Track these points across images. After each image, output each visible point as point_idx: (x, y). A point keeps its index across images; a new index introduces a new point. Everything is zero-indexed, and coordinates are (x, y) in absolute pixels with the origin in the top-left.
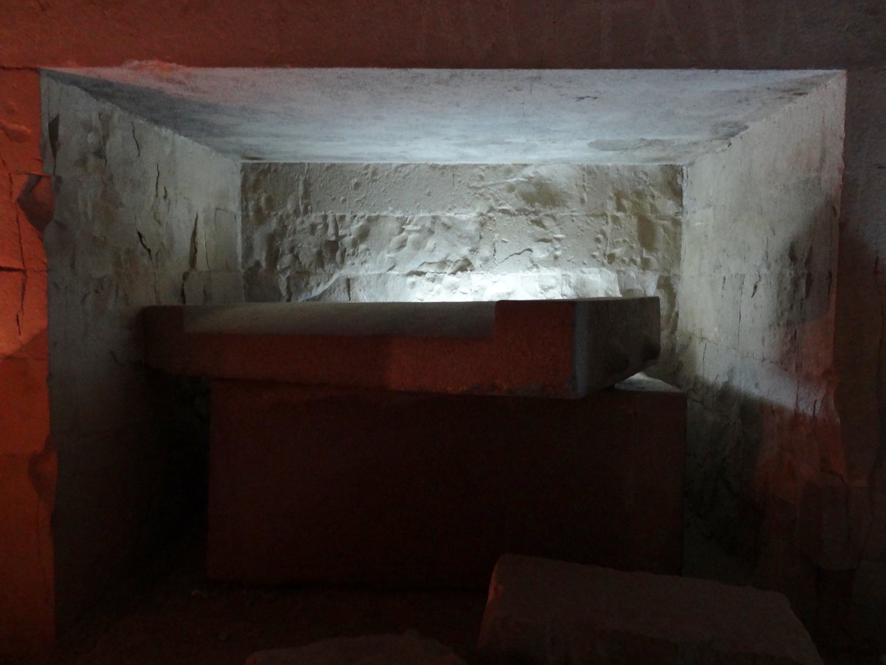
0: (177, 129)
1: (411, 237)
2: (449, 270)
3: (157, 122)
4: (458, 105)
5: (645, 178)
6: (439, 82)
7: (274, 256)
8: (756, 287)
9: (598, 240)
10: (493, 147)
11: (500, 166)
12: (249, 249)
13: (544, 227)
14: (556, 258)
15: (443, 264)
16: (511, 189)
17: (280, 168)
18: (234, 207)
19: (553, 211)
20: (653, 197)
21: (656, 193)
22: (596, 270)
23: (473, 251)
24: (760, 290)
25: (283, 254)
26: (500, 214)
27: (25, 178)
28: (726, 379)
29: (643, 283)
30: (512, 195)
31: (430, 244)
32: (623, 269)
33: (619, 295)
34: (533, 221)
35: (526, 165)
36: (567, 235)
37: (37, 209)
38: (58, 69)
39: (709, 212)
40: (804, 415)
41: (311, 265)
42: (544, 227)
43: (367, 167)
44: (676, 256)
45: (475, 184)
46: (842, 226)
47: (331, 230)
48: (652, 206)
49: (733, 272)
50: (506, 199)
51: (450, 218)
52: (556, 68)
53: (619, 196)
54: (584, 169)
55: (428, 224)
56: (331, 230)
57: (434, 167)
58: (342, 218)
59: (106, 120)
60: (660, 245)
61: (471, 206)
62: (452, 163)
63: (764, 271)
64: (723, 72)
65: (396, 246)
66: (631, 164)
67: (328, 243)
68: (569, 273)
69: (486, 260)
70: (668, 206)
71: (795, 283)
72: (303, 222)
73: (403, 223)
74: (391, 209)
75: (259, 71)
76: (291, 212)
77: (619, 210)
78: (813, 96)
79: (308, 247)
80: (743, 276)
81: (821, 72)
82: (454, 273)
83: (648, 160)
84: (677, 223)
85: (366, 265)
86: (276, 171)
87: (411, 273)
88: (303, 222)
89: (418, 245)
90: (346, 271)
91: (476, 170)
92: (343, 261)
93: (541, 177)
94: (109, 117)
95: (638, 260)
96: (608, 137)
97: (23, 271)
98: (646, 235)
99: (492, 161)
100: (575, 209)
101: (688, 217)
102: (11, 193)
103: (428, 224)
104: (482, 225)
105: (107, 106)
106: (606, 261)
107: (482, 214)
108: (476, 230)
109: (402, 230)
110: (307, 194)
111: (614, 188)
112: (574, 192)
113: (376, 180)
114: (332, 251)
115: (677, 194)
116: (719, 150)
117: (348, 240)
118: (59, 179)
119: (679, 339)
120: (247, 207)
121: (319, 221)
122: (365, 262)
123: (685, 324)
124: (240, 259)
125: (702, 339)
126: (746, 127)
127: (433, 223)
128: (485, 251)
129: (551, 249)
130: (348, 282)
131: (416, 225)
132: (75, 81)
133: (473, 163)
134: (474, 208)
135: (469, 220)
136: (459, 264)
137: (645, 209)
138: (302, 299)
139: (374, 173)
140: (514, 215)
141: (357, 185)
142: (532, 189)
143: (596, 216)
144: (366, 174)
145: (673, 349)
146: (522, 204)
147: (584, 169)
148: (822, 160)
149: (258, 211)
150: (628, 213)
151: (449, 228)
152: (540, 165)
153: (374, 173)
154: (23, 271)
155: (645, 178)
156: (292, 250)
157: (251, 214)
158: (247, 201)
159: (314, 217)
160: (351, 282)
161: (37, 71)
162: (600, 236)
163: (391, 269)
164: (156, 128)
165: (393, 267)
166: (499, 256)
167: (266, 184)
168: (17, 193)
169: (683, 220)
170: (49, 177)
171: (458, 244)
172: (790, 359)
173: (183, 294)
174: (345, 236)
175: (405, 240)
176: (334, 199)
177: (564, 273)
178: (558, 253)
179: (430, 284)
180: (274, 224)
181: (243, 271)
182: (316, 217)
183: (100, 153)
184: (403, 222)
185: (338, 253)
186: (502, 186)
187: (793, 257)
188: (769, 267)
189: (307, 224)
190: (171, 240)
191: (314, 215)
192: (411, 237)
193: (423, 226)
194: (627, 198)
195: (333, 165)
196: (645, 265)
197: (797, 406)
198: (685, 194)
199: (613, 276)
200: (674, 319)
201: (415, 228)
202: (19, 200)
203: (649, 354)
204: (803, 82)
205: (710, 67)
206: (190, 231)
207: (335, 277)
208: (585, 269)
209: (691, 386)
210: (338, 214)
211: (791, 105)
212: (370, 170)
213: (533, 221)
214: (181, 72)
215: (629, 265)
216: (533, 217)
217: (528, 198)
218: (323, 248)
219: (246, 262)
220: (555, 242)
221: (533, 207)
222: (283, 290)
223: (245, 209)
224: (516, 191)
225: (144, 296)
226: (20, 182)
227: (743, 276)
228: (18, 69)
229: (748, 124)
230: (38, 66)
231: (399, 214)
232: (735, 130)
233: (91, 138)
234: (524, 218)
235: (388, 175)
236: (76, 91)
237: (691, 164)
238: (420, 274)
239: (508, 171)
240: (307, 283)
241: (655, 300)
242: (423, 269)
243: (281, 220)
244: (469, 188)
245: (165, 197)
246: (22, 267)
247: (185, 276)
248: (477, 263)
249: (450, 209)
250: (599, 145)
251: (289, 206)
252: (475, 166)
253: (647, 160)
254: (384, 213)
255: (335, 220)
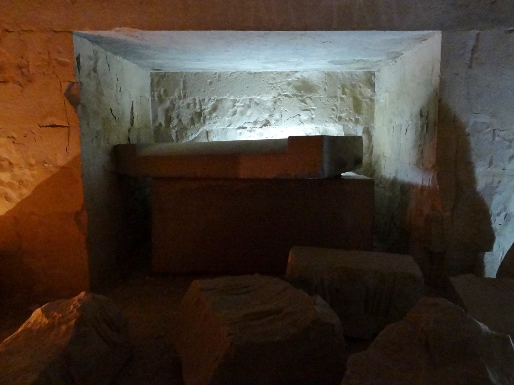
0: (124, 57)
1: (239, 109)
2: (259, 126)
3: (116, 54)
4: (266, 45)
5: (356, 77)
6: (259, 36)
7: (169, 120)
8: (407, 130)
9: (333, 110)
10: (281, 63)
11: (284, 72)
12: (155, 117)
13: (306, 103)
14: (312, 119)
15: (256, 123)
16: (289, 84)
17: (170, 74)
18: (148, 95)
19: (311, 95)
20: (360, 87)
21: (362, 85)
22: (332, 124)
23: (271, 116)
24: (408, 131)
25: (173, 119)
26: (284, 97)
27: (67, 84)
28: (394, 175)
29: (356, 131)
30: (290, 87)
31: (249, 112)
32: (346, 124)
33: (343, 134)
34: (300, 100)
35: (296, 72)
36: (317, 107)
37: (73, 98)
38: (80, 32)
39: (387, 94)
40: (425, 186)
41: (188, 124)
42: (306, 103)
43: (216, 73)
44: (372, 118)
45: (271, 82)
46: (440, 101)
47: (198, 106)
48: (360, 92)
49: (397, 124)
50: (287, 89)
51: (258, 99)
52: (313, 30)
53: (343, 87)
54: (326, 74)
55: (248, 103)
56: (198, 106)
57: (250, 73)
58: (204, 100)
59: (96, 53)
60: (364, 111)
61: (264, 93)
62: (259, 71)
63: (410, 122)
64: (388, 32)
65: (232, 114)
66: (349, 70)
67: (196, 113)
68: (319, 126)
69: (277, 120)
70: (368, 92)
71: (422, 127)
72: (183, 103)
73: (235, 102)
74: (228, 95)
75: (175, 32)
76: (177, 97)
77: (343, 94)
78: (429, 41)
79: (186, 116)
80: (401, 125)
81: (430, 31)
82: (261, 127)
83: (358, 69)
84: (372, 100)
85: (216, 124)
86: (168, 76)
87: (240, 128)
88: (183, 103)
89: (243, 114)
90: (206, 128)
91: (271, 75)
92: (204, 122)
93: (305, 78)
94: (97, 52)
95: (353, 119)
96: (337, 58)
97: (69, 127)
98: (357, 107)
99: (279, 70)
100: (321, 94)
101: (378, 97)
102: (61, 91)
103: (248, 103)
104: (275, 102)
105: (96, 47)
106: (337, 120)
107: (275, 97)
108: (272, 105)
109: (234, 106)
110: (185, 88)
111: (341, 83)
112: (322, 86)
113: (220, 80)
114: (199, 117)
115: (372, 85)
116: (391, 64)
117: (207, 111)
118: (81, 83)
119: (374, 158)
120: (154, 94)
121: (192, 102)
122: (216, 122)
123: (376, 151)
124: (151, 122)
125: (384, 157)
126: (402, 54)
127: (250, 102)
128: (277, 116)
129: (310, 114)
130: (207, 133)
131: (241, 103)
132: (86, 37)
133: (269, 71)
134: (271, 94)
135: (268, 100)
136: (264, 122)
137: (356, 93)
138: (184, 141)
139: (219, 76)
140: (291, 97)
141: (211, 83)
142: (300, 84)
143: (332, 97)
144: (215, 77)
145: (371, 164)
146: (295, 92)
147: (326, 74)
148: (433, 71)
149: (160, 96)
150: (348, 95)
151: (258, 104)
152: (304, 72)
153: (219, 76)
154: (69, 127)
155: (356, 77)
156: (178, 117)
157: (156, 98)
158: (154, 91)
159: (189, 100)
160: (209, 133)
161: (71, 33)
162: (334, 107)
163: (229, 126)
164: (115, 57)
165: (230, 125)
166: (284, 118)
167: (162, 82)
168: (64, 91)
169: (375, 99)
170: (77, 83)
171: (263, 112)
172: (420, 163)
173: (129, 139)
174: (205, 109)
175: (236, 111)
176: (199, 90)
177: (317, 126)
178: (313, 116)
179: (249, 133)
180: (168, 104)
181: (153, 128)
182: (190, 100)
183: (95, 70)
184: (235, 101)
185: (202, 118)
186: (284, 83)
187: (421, 116)
188: (412, 121)
189: (185, 104)
190: (123, 112)
191: (189, 99)
192: (239, 109)
193: (245, 104)
194: (348, 89)
195: (198, 73)
196: (357, 121)
197: (423, 183)
198: (376, 86)
199: (341, 127)
200: (371, 148)
201: (241, 105)
202: (65, 94)
203: (356, 163)
204: (424, 35)
205: (382, 30)
206: (131, 107)
207: (200, 130)
208: (327, 124)
209: (379, 181)
210: (201, 98)
211: (421, 44)
212: (217, 75)
213: (300, 100)
214: (138, 32)
215: (349, 122)
216: (301, 98)
217: (298, 89)
218: (194, 116)
219: (154, 124)
220: (312, 110)
221: (301, 93)
222: (174, 137)
223: (153, 96)
224: (292, 85)
225: (118, 138)
226: (65, 86)
227: (401, 125)
228: (63, 32)
229: (403, 52)
230: (72, 30)
231: (232, 98)
232: (398, 55)
233: (92, 63)
234: (296, 98)
235: (226, 78)
236: (85, 40)
237: (379, 71)
238: (244, 128)
239: (288, 75)
240: (186, 134)
241: (360, 138)
242: (245, 126)
243: (172, 102)
244: (268, 84)
245: (120, 91)
246: (68, 125)
247: (129, 130)
248: (273, 122)
249: (258, 95)
250: (332, 62)
251: (176, 94)
252: (271, 72)
253: (357, 69)
254: (225, 97)
255: (200, 101)
